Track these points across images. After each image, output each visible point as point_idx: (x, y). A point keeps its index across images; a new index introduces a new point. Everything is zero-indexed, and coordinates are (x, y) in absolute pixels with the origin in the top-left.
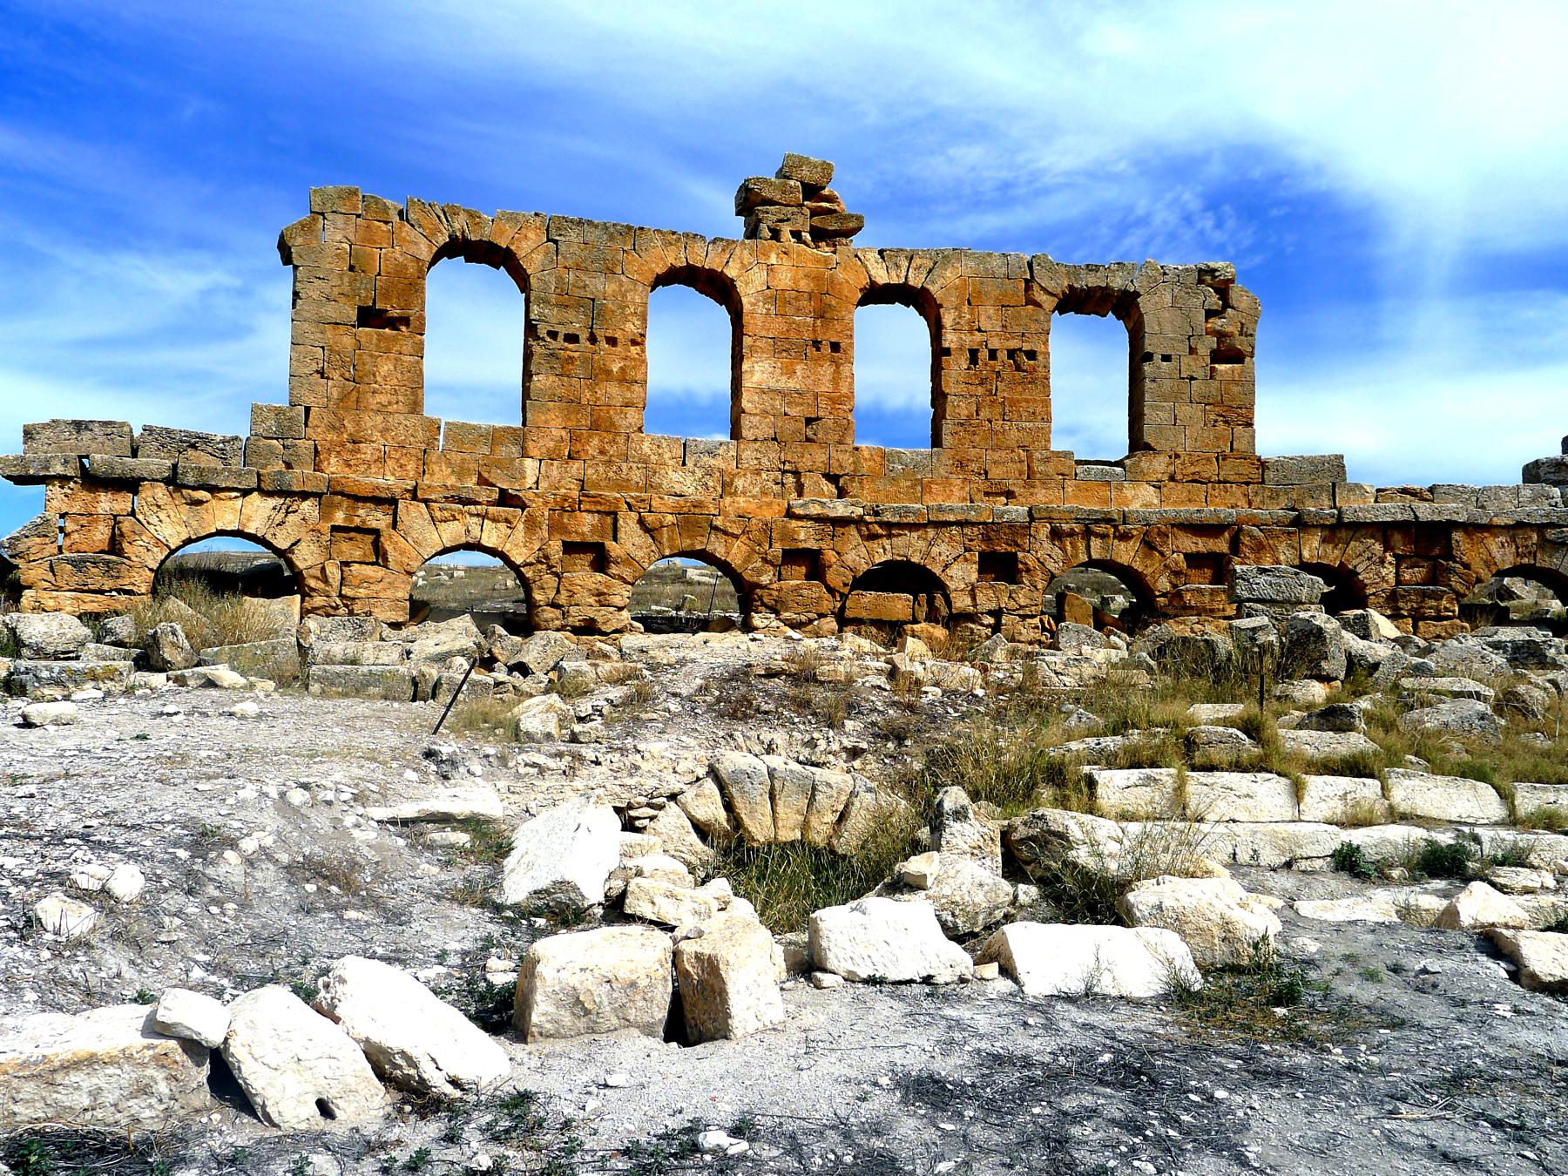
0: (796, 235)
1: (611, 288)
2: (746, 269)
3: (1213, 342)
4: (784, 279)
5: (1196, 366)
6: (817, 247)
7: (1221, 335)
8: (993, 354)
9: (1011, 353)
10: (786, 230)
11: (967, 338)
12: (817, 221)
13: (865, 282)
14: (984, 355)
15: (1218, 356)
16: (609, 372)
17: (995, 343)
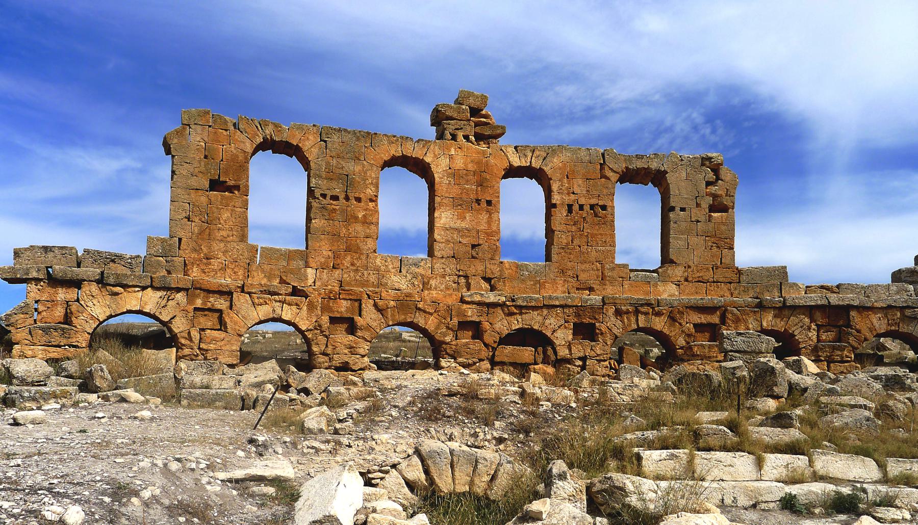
0: (466, 137)
1: (358, 168)
2: (436, 157)
3: (710, 200)
4: (459, 163)
5: (700, 214)
6: (479, 145)
7: (715, 196)
8: (581, 207)
9: (592, 207)
10: (460, 135)
11: (566, 198)
12: (478, 129)
13: (506, 165)
14: (576, 207)
15: (713, 209)
16: (356, 218)
17: (582, 201)
